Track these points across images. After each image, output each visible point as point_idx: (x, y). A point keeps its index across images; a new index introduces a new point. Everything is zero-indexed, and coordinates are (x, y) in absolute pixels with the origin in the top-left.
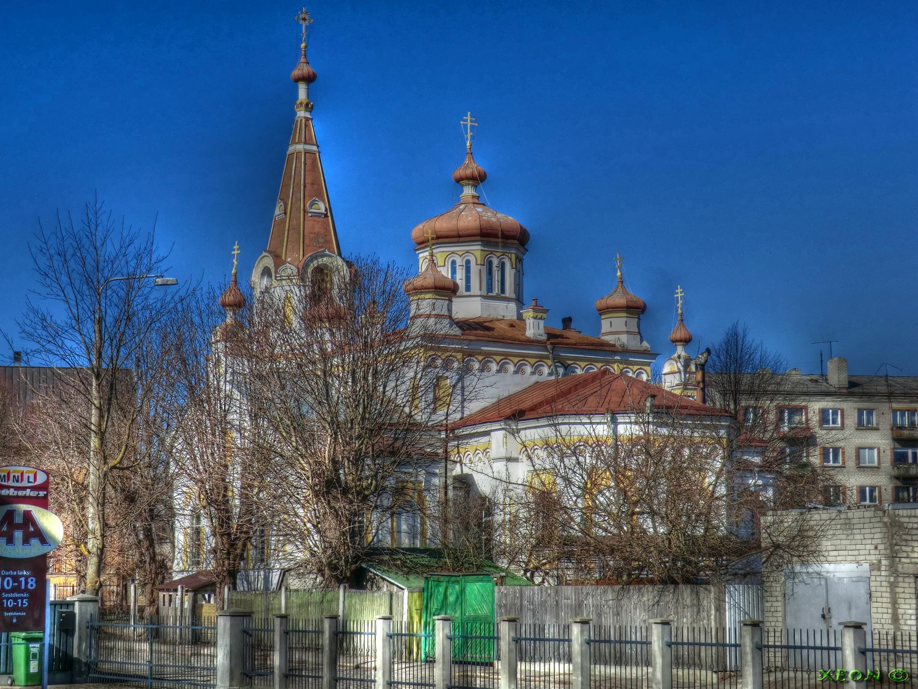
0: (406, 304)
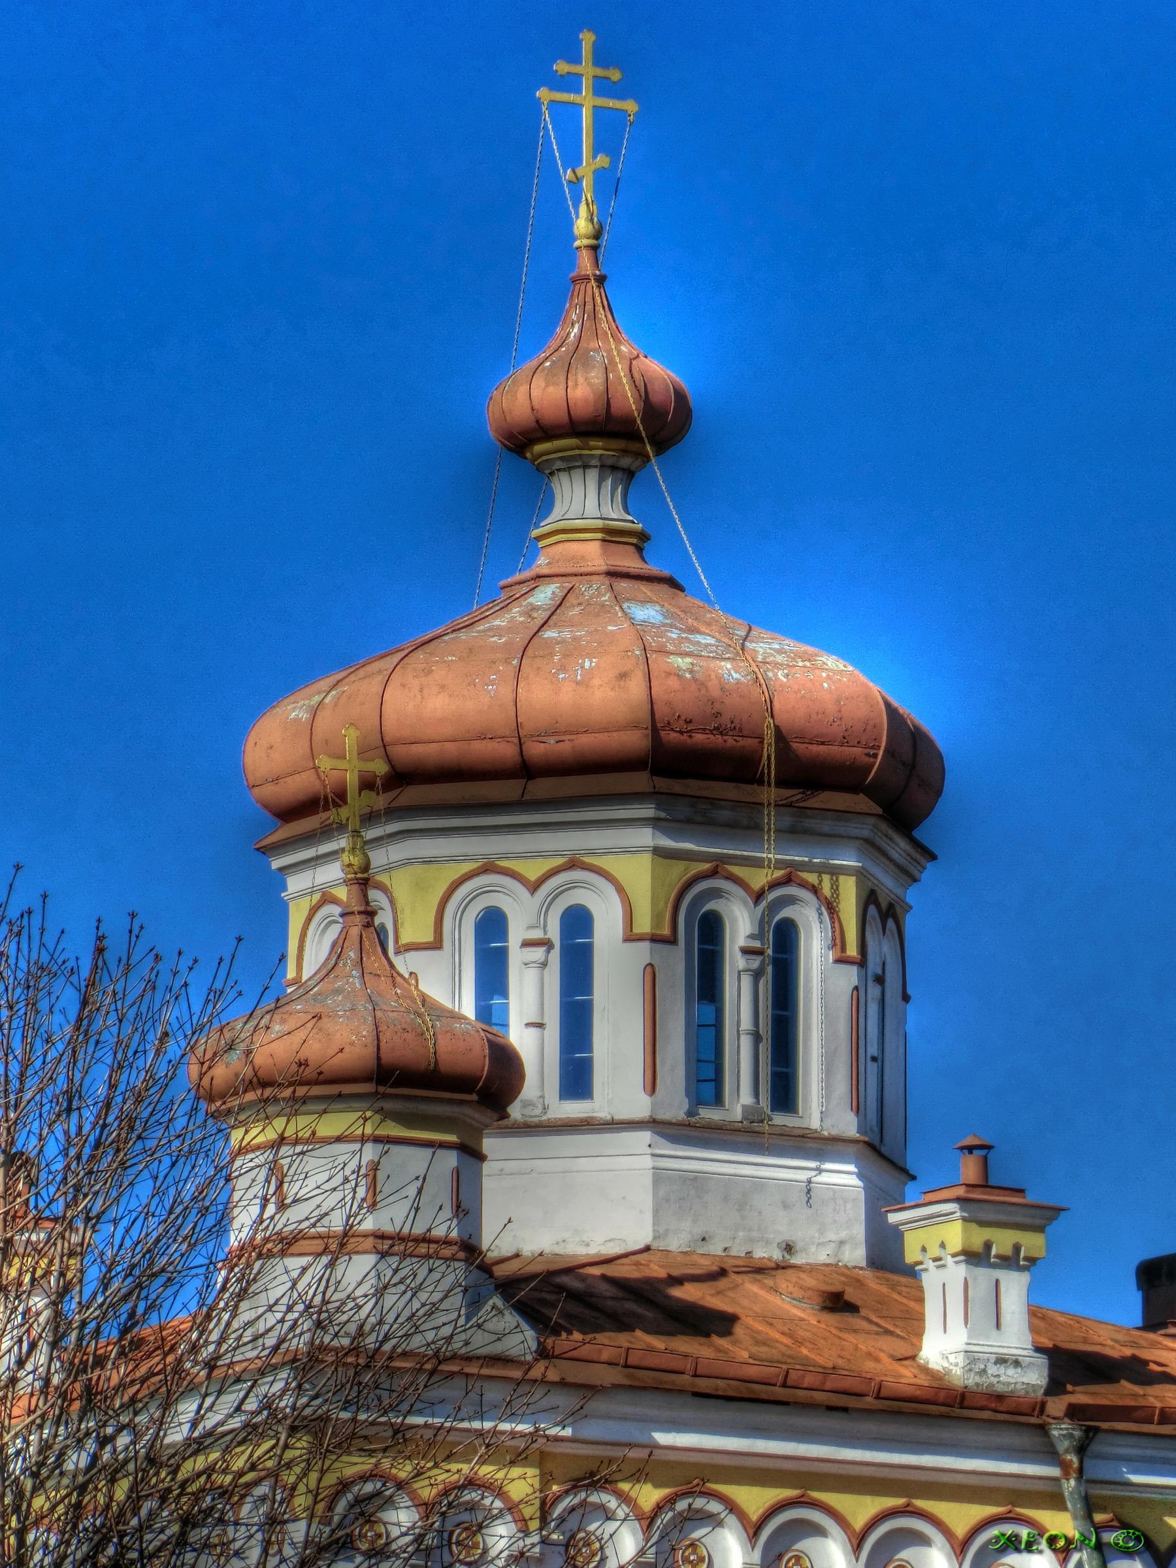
0: (205, 1170)
